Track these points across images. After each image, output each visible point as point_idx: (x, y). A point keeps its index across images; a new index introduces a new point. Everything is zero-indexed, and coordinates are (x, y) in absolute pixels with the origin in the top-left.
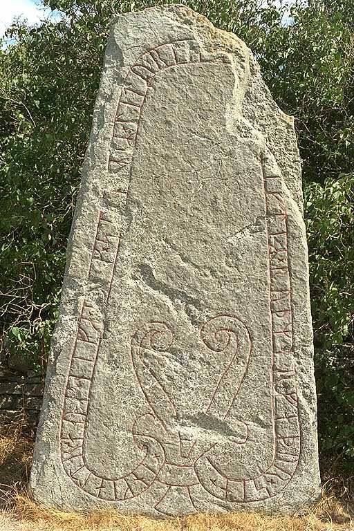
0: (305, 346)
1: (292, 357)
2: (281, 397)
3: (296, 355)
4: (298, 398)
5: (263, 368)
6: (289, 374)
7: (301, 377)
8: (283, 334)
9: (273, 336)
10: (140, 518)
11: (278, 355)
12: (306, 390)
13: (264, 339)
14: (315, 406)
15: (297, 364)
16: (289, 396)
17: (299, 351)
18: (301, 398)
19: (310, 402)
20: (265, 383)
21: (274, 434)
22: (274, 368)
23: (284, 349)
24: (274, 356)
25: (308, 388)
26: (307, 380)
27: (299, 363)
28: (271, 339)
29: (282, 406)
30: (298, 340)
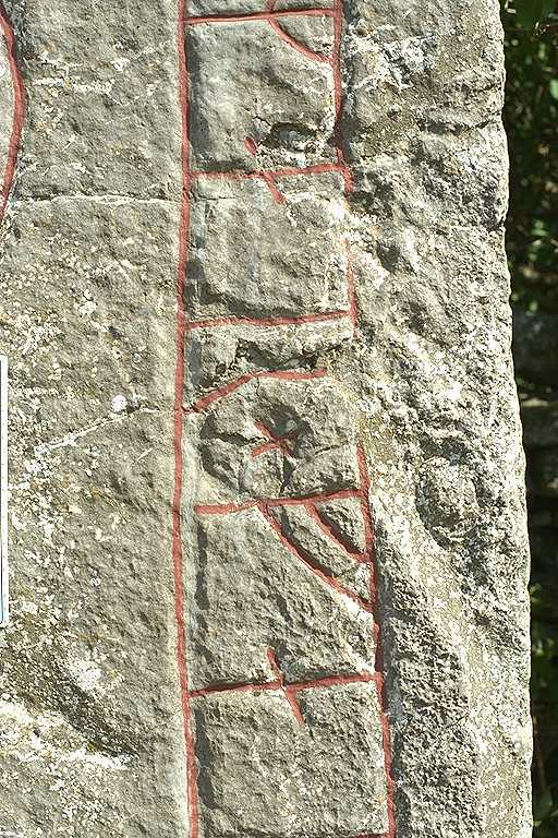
0: (438, 128)
1: (337, 209)
2: (243, 524)
3: (372, 198)
4: (376, 531)
5: (103, 282)
6: (311, 335)
7: (403, 367)
8: (262, 24)
9: (189, 43)
10: (385, 473)
11: (220, 190)
12: (448, 475)
13: (120, 62)
14: (515, 601)
15: (372, 263)
16: (300, 513)
17: (391, 165)
18: (403, 530)
20: (119, 402)
21: (183, 810)
22: (192, 286)
23: (280, 134)
24: (192, 193)
25: (455, 451)
26: (450, 393)
27: (390, 257)
28: (173, 69)
29: (247, 587)
30: (381, 70)
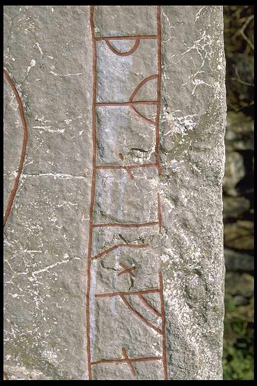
3: (170, 177)
4: (164, 304)
8: (127, 108)
11: (108, 176)
19: (202, 316)
29: (115, 325)
